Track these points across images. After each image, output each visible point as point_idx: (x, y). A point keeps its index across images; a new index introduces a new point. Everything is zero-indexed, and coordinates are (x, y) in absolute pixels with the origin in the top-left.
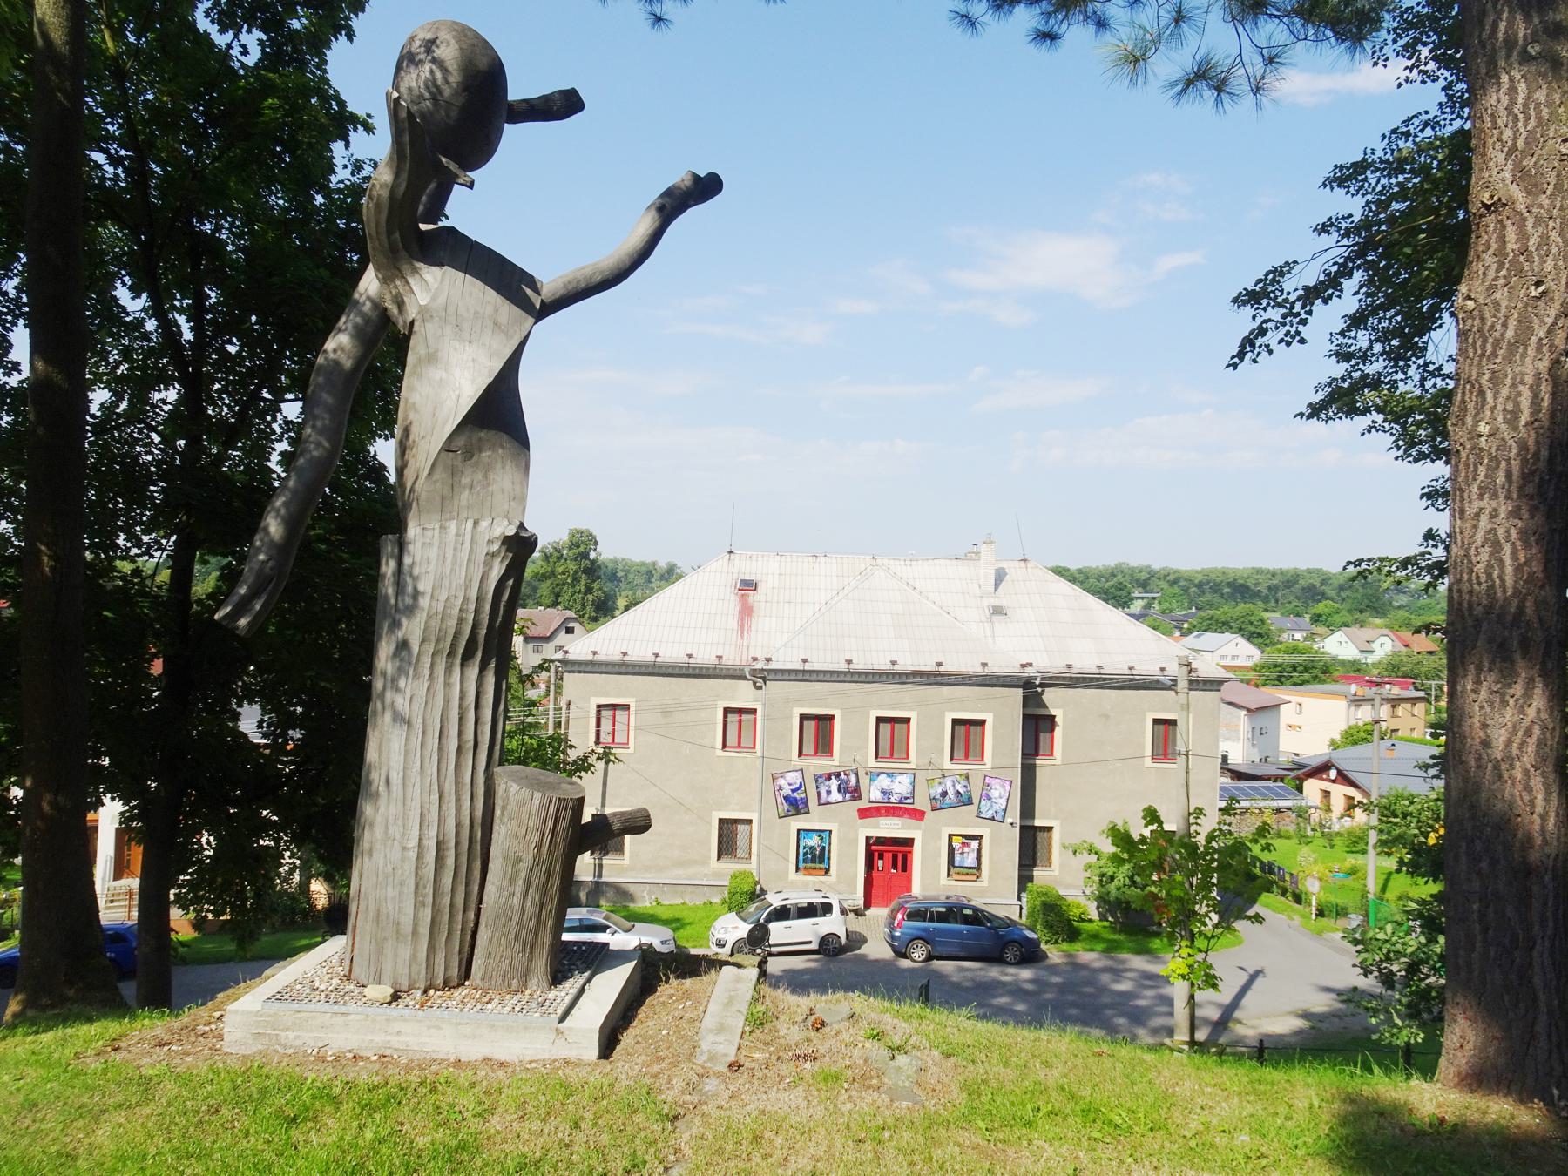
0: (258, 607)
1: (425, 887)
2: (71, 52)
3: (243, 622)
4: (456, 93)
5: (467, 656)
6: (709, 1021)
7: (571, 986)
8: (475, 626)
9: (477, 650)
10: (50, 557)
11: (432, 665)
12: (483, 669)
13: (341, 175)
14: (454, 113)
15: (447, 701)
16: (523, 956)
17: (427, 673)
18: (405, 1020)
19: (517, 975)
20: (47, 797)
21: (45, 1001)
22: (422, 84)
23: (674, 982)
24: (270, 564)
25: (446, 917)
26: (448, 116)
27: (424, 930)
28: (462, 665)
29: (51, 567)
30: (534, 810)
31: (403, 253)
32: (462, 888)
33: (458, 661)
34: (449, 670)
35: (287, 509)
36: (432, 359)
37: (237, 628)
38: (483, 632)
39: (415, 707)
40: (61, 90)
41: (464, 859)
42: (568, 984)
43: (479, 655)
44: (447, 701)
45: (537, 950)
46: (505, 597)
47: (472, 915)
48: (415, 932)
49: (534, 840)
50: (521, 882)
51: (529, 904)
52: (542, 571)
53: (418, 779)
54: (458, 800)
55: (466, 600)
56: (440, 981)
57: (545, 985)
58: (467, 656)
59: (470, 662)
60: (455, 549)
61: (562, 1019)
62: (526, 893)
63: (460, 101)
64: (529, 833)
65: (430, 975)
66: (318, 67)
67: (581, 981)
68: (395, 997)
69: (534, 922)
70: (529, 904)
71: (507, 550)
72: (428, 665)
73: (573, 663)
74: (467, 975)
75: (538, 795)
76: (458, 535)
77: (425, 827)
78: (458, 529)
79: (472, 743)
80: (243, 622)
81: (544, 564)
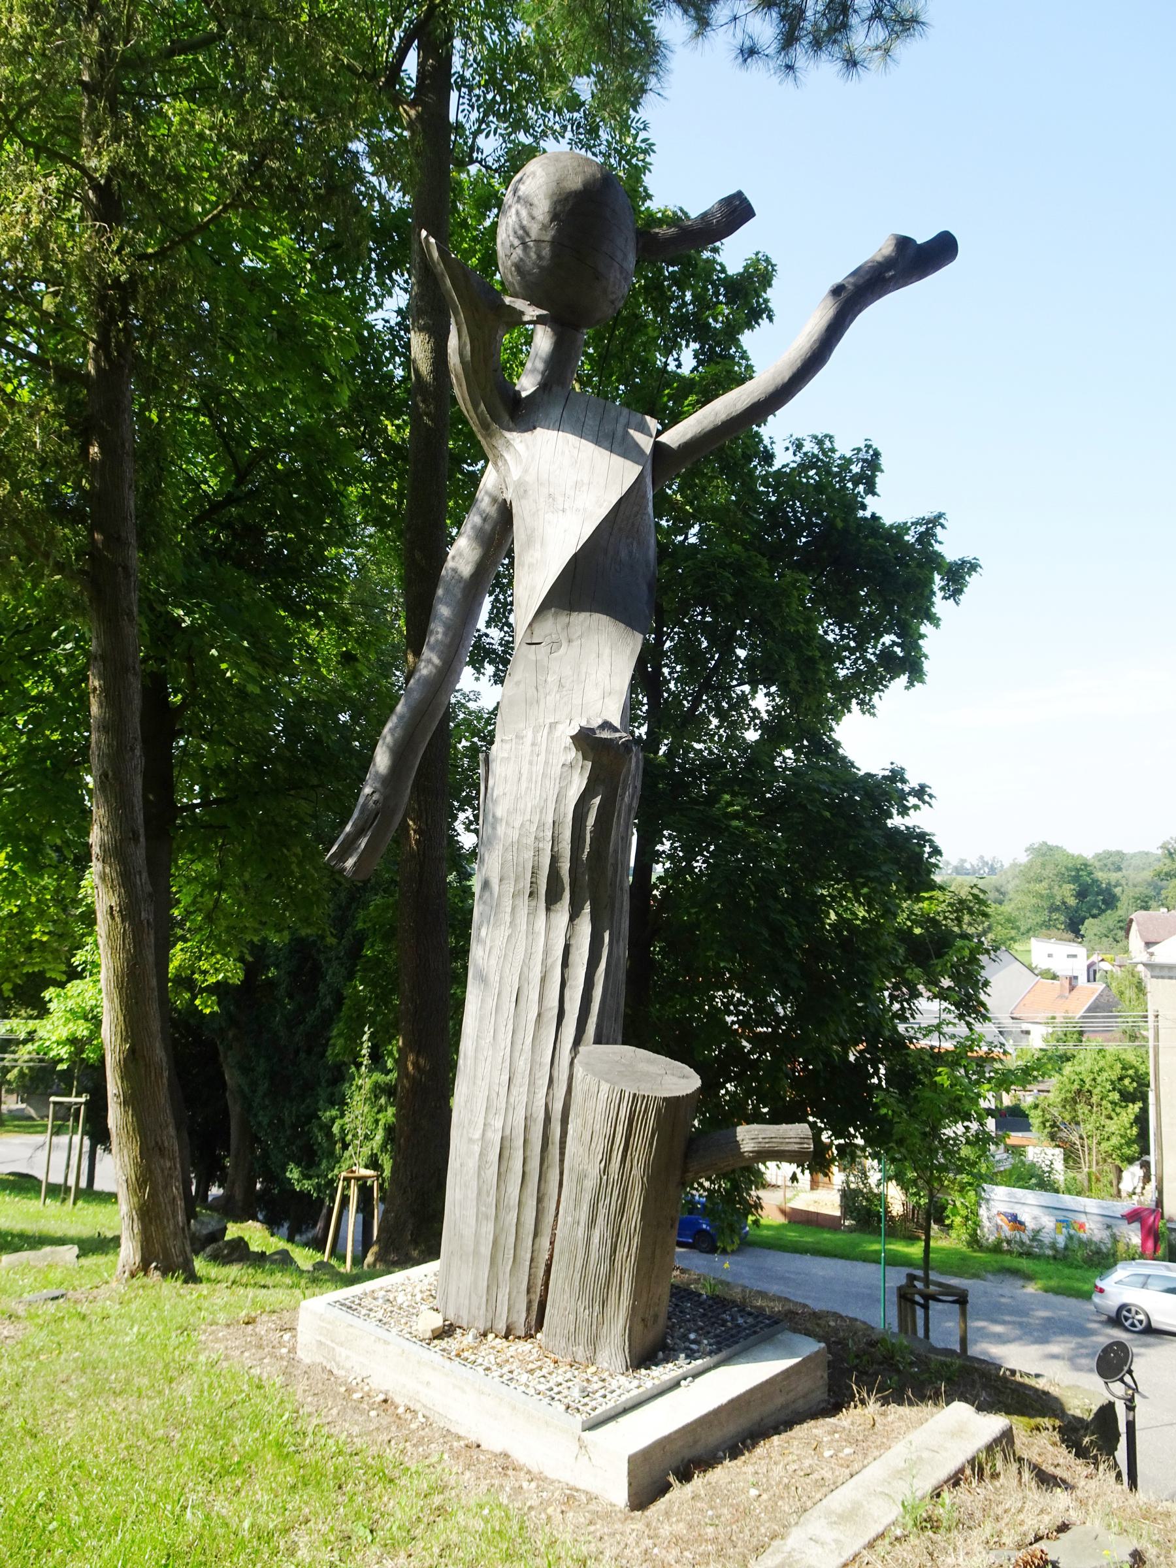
0: (363, 846)
1: (488, 1195)
2: (434, 379)
3: (350, 863)
4: (544, 228)
5: (552, 898)
6: (839, 1500)
7: (663, 1373)
8: (554, 859)
9: (563, 890)
10: (415, 832)
11: (513, 909)
12: (574, 916)
13: (783, 459)
14: (546, 251)
15: (529, 956)
16: (591, 1315)
17: (508, 918)
18: (434, 1369)
19: (582, 1339)
20: (411, 1057)
21: (393, 1257)
22: (511, 233)
23: (873, 1407)
24: (376, 797)
25: (512, 1239)
26: (539, 257)
27: (486, 1250)
28: (548, 909)
29: (416, 840)
30: (601, 1105)
31: (495, 426)
32: (531, 1203)
33: (542, 904)
34: (532, 913)
35: (393, 735)
36: (530, 542)
37: (344, 869)
38: (565, 866)
39: (493, 962)
40: (427, 415)
41: (535, 1163)
42: (656, 1371)
43: (567, 895)
44: (529, 956)
45: (609, 1310)
46: (591, 820)
47: (545, 1242)
48: (476, 1252)
49: (600, 1146)
50: (585, 1207)
51: (596, 1240)
52: (1166, 869)
53: (490, 1053)
54: (532, 1083)
55: (541, 826)
56: (501, 1327)
57: (620, 1361)
58: (552, 898)
59: (558, 905)
60: (531, 763)
61: (594, 1425)
62: (592, 1223)
63: (548, 236)
64: (595, 1139)
65: (490, 1316)
66: (742, 358)
67: (678, 1372)
68: (445, 1332)
69: (604, 1269)
70: (596, 1240)
71: (585, 758)
72: (509, 909)
73: (1162, 967)
74: (540, 1325)
75: (605, 1087)
76: (533, 744)
77: (491, 1116)
78: (535, 737)
79: (556, 1011)
80: (350, 863)
81: (1167, 861)
